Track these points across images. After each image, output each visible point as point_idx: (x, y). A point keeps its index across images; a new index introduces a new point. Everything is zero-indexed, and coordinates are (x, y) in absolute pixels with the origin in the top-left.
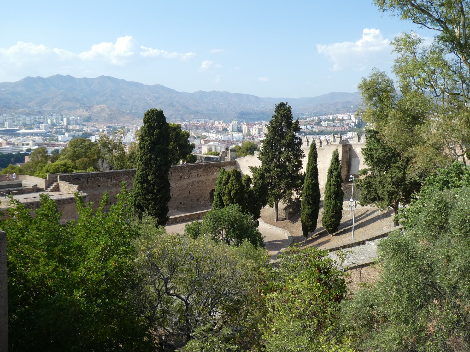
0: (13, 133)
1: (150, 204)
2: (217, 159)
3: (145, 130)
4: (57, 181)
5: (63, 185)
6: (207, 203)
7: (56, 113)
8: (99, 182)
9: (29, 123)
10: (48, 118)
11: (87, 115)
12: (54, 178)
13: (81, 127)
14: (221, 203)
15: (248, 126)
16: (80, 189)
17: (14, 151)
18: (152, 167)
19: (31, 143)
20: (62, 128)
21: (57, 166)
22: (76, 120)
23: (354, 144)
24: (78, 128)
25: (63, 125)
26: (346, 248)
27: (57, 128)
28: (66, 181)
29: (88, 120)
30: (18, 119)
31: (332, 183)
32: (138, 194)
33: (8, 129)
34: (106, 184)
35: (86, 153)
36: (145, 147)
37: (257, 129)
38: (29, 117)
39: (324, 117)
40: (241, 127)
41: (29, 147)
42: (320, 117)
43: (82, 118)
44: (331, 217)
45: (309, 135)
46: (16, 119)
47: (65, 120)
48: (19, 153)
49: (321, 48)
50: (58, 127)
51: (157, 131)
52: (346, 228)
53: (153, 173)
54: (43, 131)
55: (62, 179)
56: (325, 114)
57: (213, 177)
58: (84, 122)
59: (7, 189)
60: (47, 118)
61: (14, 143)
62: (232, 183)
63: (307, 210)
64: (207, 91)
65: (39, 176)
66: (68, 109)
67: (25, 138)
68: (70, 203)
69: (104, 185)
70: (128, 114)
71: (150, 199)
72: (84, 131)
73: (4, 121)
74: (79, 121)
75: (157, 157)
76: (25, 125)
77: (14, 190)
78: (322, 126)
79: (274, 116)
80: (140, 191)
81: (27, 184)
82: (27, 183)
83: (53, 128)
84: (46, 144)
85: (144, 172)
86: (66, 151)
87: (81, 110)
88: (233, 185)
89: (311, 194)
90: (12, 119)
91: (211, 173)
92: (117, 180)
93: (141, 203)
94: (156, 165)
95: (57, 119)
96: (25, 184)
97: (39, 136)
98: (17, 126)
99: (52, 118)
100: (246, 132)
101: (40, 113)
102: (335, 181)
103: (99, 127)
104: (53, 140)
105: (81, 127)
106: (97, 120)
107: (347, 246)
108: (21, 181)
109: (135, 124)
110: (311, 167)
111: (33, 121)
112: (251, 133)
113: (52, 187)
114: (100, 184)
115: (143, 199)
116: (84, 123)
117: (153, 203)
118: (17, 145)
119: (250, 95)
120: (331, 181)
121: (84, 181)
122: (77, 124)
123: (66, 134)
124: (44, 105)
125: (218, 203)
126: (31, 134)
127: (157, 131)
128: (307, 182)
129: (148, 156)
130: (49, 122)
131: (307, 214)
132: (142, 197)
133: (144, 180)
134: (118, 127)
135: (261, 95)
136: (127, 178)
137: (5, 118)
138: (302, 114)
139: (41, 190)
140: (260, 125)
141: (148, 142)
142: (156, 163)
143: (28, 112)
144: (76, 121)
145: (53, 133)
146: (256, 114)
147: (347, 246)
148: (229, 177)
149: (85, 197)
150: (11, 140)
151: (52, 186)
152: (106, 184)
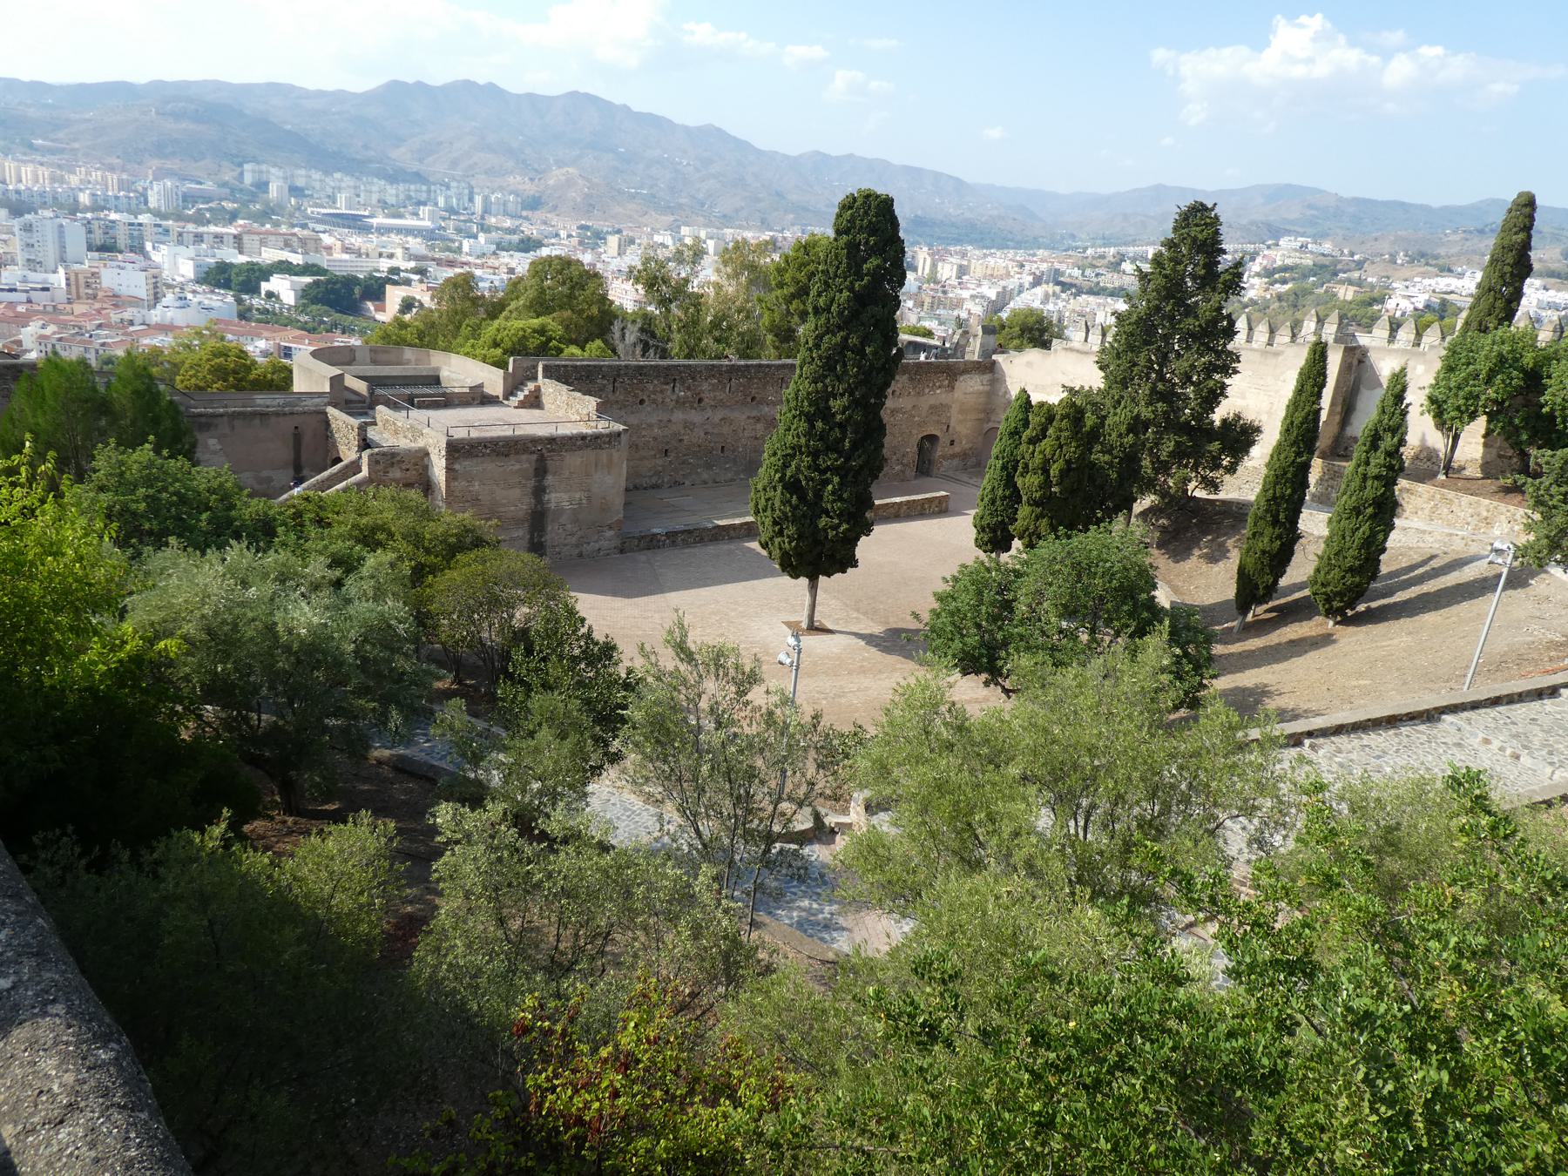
0: (354, 223)
1: (827, 482)
3: (836, 257)
4: (535, 378)
5: (553, 391)
7: (459, 182)
12: (528, 369)
13: (517, 223)
14: (1007, 493)
16: (602, 410)
17: (362, 269)
18: (845, 372)
19: (399, 252)
21: (521, 333)
23: (1375, 348)
24: (508, 223)
25: (473, 214)
26: (1502, 705)
28: (558, 380)
29: (534, 204)
30: (368, 187)
31: (1373, 470)
32: (793, 448)
33: (344, 211)
34: (659, 398)
35: (571, 296)
36: (834, 308)
40: (913, 257)
42: (1123, 249)
44: (1347, 572)
45: (1087, 293)
49: (1160, 55)
50: (462, 218)
51: (875, 263)
52: (1374, 605)
53: (845, 391)
54: (427, 224)
55: (550, 373)
56: (1133, 243)
57: (932, 401)
58: (523, 208)
59: (407, 391)
62: (1058, 438)
63: (1266, 540)
64: (833, 154)
65: (475, 357)
66: (486, 173)
67: (384, 238)
68: (580, 448)
69: (654, 402)
70: (633, 197)
71: (828, 469)
74: (511, 207)
75: (865, 341)
77: (423, 396)
78: (1124, 272)
79: (1170, 244)
80: (803, 440)
82: (454, 376)
84: (434, 260)
85: (820, 385)
86: (521, 287)
88: (1061, 446)
89: (1290, 495)
90: (355, 187)
91: (927, 391)
92: (689, 388)
93: (801, 477)
95: (459, 196)
97: (416, 236)
99: (449, 193)
100: (927, 270)
101: (418, 177)
102: (1385, 466)
103: (560, 225)
104: (449, 249)
105: (517, 223)
106: (555, 207)
107: (1505, 700)
108: (438, 369)
109: (646, 226)
110: (1303, 414)
111: (402, 196)
112: (939, 275)
113: (521, 396)
115: (809, 467)
116: (524, 213)
117: (836, 479)
118: (367, 255)
119: (942, 174)
120: (1367, 463)
121: (604, 386)
122: (506, 213)
123: (482, 237)
124: (430, 159)
125: (1000, 492)
126: (399, 230)
128: (1283, 456)
129: (839, 339)
130: (441, 202)
131: (1264, 552)
132: (807, 460)
133: (818, 408)
134: (605, 229)
135: (971, 176)
137: (338, 184)
138: (1073, 237)
140: (964, 255)
141: (846, 294)
142: (860, 361)
144: (504, 205)
145: (450, 232)
146: (953, 225)
147: (1505, 700)
148: (1050, 419)
149: (619, 434)
152: (659, 398)
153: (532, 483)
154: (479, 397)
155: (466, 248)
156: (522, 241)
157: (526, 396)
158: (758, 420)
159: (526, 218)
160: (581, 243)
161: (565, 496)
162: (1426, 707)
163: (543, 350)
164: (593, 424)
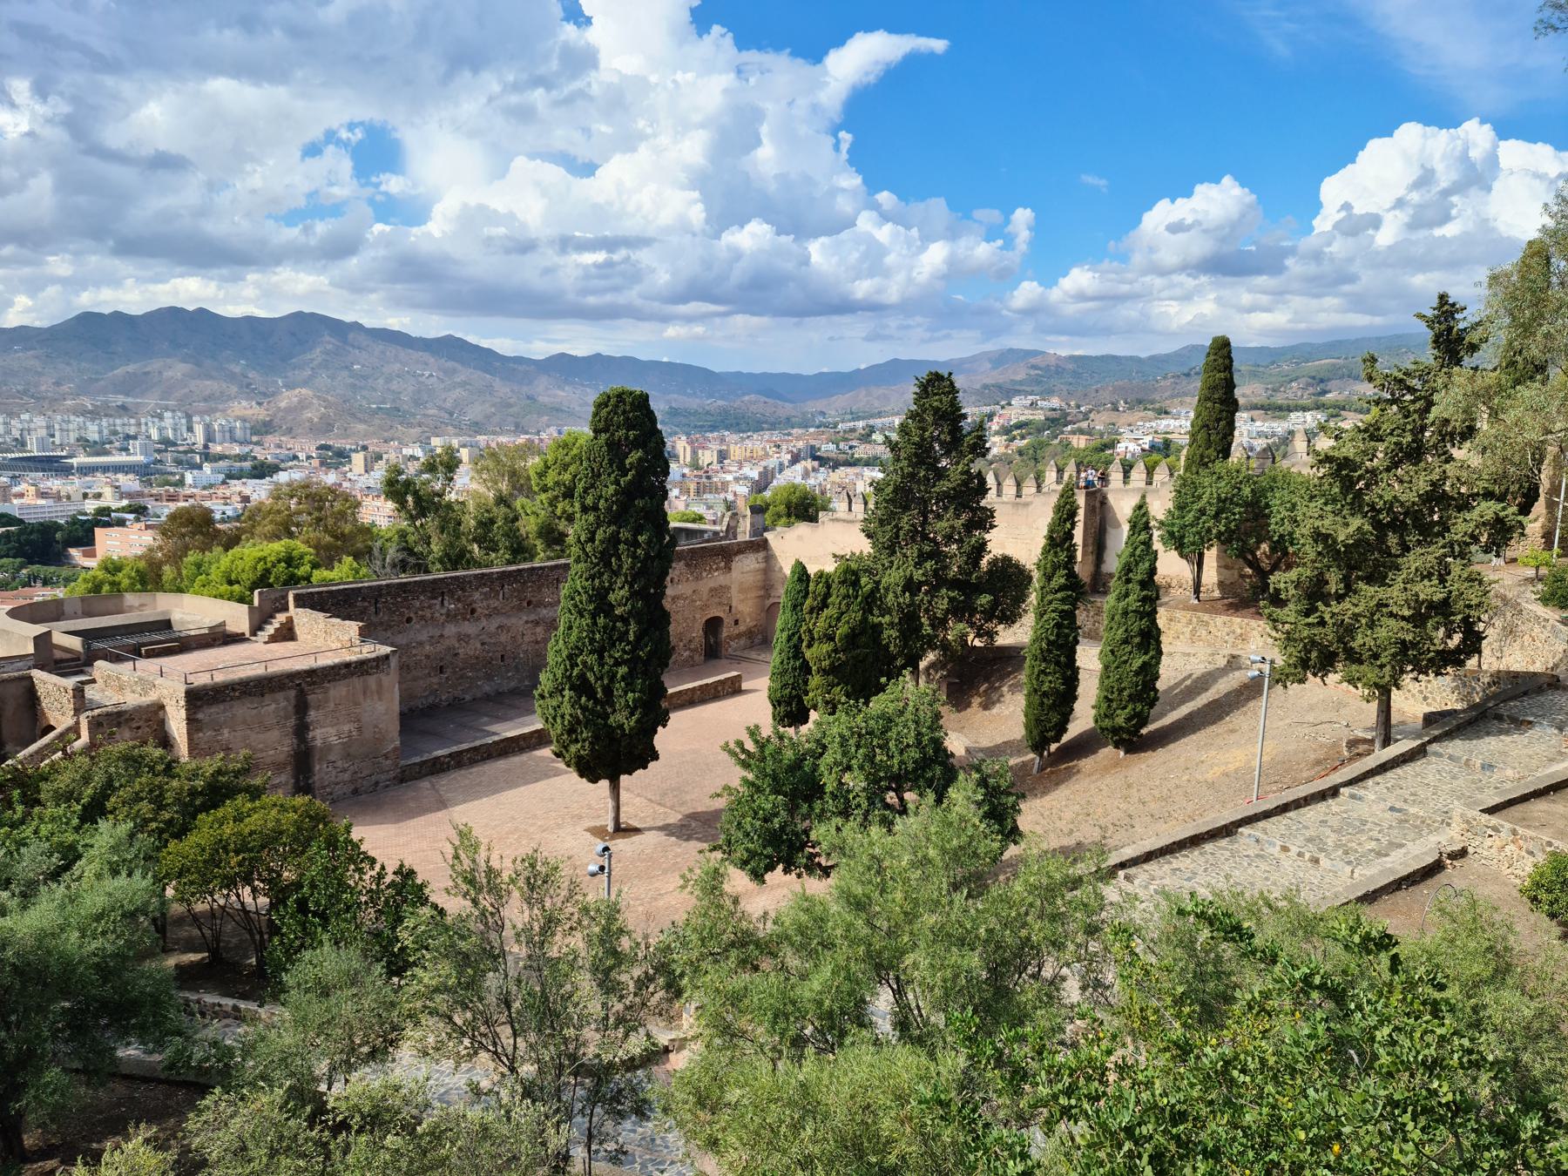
2: (716, 533)
4: (286, 609)
5: (307, 622)
6: (696, 657)
8: (408, 608)
9: (96, 437)
10: (150, 424)
11: (261, 417)
15: (691, 443)
16: (365, 634)
17: (60, 514)
19: (108, 492)
20: (193, 451)
22: (231, 431)
27: (179, 452)
37: (715, 453)
38: (97, 422)
39: (878, 422)
41: (102, 503)
42: (871, 422)
43: (248, 425)
46: (57, 427)
47: (199, 430)
48: (74, 521)
50: (181, 449)
54: (139, 458)
55: (301, 602)
56: (880, 415)
60: (146, 424)
61: (59, 492)
67: (87, 479)
68: (345, 677)
69: (423, 618)
72: (255, 458)
73: (26, 433)
74: (239, 434)
75: (637, 531)
76: (86, 444)
81: (189, 623)
83: (166, 451)
85: (597, 582)
87: (244, 403)
91: (704, 574)
92: (459, 600)
94: (634, 557)
96: (182, 622)
97: (127, 473)
98: (62, 448)
99: (163, 424)
100: (688, 459)
103: (297, 447)
105: (247, 449)
111: (106, 432)
113: (270, 630)
114: (412, 615)
116: (255, 439)
118: (69, 497)
121: (366, 608)
122: (233, 440)
126: (105, 469)
127: (634, 456)
136: (485, 594)
139: (237, 639)
143: (90, 407)
144: (230, 431)
146: (708, 413)
149: (387, 657)
150: (49, 484)
151: (271, 623)
153: (292, 722)
154: (220, 637)
155: (189, 478)
156: (254, 468)
157: (276, 630)
158: (537, 623)
159: (257, 443)
160: (322, 464)
161: (332, 731)
162: (1223, 823)
163: (292, 580)
164: (358, 649)
